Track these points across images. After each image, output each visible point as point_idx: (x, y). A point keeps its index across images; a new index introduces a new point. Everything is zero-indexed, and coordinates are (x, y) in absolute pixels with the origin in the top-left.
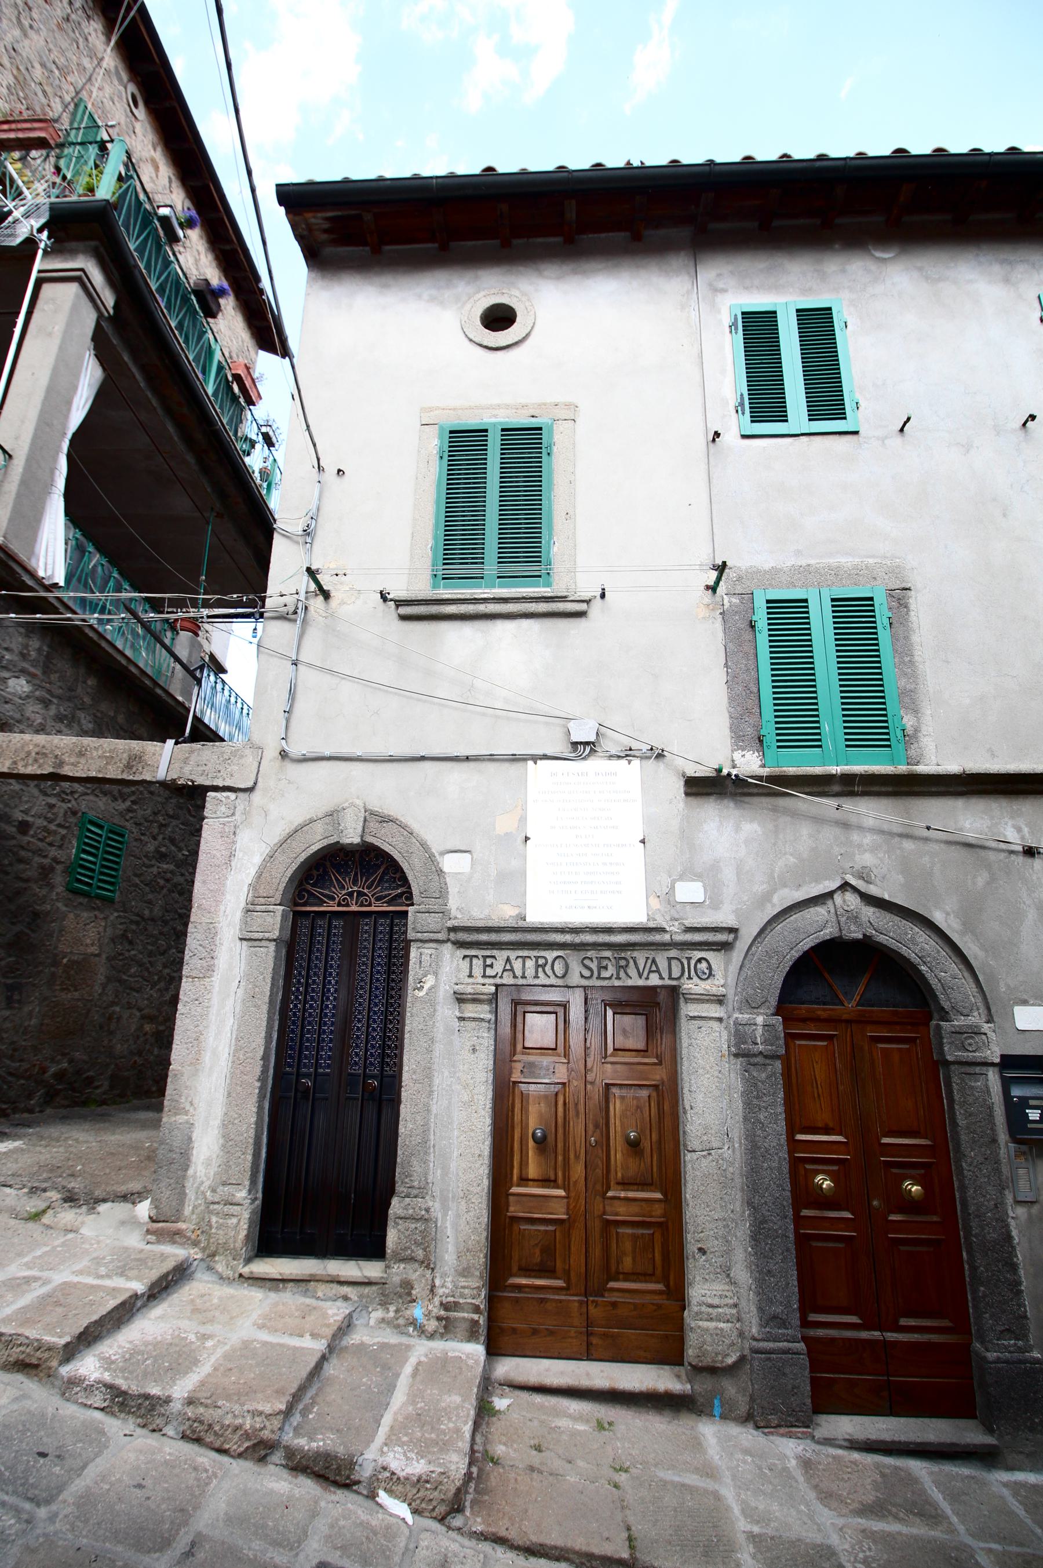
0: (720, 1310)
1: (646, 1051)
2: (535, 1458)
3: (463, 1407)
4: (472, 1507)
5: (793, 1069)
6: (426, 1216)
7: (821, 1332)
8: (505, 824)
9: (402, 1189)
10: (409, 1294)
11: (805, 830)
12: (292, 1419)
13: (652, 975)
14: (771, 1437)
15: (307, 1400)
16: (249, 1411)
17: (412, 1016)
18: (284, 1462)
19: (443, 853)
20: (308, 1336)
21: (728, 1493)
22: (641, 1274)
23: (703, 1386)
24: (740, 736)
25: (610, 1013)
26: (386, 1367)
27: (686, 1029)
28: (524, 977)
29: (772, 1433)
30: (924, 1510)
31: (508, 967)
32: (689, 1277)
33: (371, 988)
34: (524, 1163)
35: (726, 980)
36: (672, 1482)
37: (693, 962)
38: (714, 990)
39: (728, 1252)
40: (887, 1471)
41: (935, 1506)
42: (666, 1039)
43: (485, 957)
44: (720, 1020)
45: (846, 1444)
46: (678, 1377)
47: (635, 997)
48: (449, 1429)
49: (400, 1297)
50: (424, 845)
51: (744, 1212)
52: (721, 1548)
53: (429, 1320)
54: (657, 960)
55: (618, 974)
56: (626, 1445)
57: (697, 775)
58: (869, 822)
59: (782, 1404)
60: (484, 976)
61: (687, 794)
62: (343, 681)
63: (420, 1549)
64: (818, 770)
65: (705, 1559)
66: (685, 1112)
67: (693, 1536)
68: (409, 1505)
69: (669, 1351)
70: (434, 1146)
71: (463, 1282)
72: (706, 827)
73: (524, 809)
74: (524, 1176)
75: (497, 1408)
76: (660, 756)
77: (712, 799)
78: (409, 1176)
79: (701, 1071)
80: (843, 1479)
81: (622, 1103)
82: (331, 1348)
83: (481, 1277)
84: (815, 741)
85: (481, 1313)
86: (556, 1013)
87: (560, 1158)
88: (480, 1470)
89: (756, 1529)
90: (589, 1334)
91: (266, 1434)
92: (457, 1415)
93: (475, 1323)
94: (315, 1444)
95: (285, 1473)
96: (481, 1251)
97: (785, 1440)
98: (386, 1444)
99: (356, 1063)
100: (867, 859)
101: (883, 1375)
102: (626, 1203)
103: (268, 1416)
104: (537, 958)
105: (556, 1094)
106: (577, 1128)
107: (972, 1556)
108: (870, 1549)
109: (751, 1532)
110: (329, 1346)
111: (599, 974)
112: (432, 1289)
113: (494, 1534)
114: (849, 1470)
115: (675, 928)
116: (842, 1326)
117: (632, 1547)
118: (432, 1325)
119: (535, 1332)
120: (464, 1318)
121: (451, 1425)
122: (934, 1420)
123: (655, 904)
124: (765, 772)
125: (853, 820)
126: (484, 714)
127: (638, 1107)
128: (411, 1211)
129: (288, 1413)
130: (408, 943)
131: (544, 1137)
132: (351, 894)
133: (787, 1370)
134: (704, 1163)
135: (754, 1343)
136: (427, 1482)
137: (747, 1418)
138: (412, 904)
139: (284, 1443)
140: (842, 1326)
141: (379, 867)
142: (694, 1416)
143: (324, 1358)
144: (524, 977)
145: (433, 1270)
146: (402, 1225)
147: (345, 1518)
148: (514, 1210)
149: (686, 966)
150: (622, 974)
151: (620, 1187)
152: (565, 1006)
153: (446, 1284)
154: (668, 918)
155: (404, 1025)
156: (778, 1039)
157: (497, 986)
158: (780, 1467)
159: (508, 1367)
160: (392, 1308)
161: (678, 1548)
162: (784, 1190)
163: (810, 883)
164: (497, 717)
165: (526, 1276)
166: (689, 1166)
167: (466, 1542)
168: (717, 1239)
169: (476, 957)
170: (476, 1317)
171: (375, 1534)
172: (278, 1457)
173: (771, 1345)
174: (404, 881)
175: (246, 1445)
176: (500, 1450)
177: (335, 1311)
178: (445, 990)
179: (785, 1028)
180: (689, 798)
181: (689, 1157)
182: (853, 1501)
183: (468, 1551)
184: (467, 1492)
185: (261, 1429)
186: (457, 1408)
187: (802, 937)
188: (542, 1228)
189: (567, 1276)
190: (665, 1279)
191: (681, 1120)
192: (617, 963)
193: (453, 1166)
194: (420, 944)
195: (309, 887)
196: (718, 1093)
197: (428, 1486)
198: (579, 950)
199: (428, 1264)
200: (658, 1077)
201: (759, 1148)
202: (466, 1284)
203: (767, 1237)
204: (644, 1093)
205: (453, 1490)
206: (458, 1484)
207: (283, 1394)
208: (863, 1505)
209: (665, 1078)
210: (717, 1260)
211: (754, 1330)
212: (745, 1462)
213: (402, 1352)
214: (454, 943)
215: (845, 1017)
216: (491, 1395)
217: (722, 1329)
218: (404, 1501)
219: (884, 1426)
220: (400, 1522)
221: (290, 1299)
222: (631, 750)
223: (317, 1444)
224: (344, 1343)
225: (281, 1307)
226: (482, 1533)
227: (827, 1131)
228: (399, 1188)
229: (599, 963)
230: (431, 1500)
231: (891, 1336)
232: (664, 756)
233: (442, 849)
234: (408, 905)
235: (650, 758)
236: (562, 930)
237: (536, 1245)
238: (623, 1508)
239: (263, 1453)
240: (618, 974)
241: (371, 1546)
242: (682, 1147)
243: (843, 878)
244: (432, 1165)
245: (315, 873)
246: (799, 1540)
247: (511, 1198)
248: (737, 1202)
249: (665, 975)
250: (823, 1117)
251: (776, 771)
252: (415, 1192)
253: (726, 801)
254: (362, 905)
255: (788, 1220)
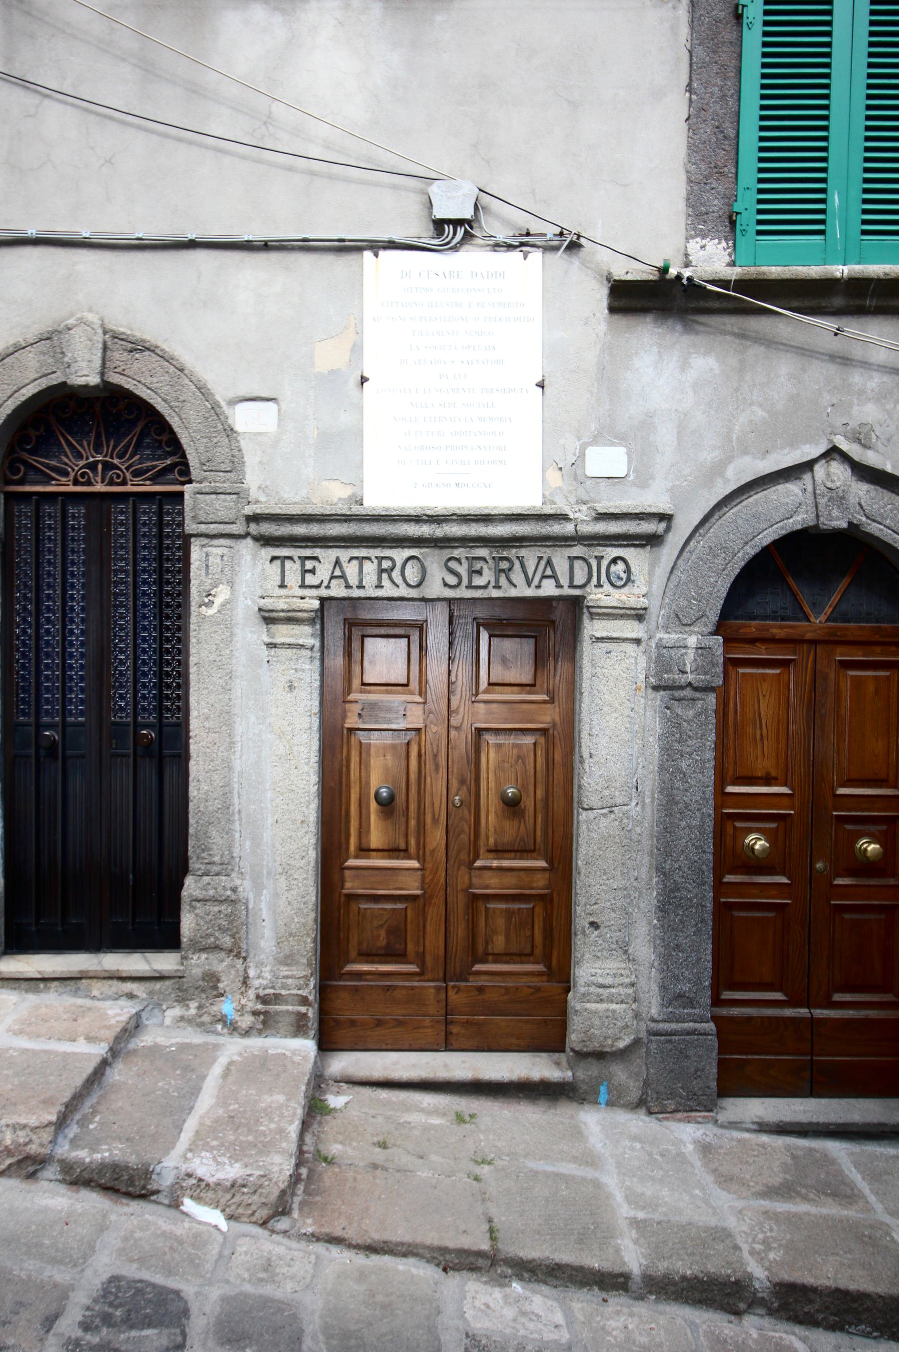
0: (613, 990)
1: (534, 685)
2: (379, 1155)
3: (287, 1106)
4: (301, 1209)
5: (731, 705)
6: (233, 897)
7: (735, 1011)
8: (329, 356)
9: (197, 866)
10: (215, 987)
11: (785, 367)
12: (67, 1131)
13: (546, 582)
14: (666, 1123)
15: (86, 1107)
16: (8, 1126)
17: (199, 642)
18: (60, 1177)
19: (232, 402)
20: (81, 1040)
21: (611, 1181)
22: (515, 954)
23: (585, 1073)
24: (701, 214)
25: (484, 636)
26: (188, 1068)
27: (588, 651)
28: (361, 587)
29: (667, 1119)
30: (839, 1190)
31: (338, 573)
32: (576, 954)
33: (135, 605)
34: (363, 830)
35: (650, 587)
36: (545, 1173)
37: (605, 563)
38: (633, 602)
39: (628, 925)
40: (800, 1153)
41: (852, 1186)
42: (562, 668)
43: (303, 559)
44: (638, 641)
45: (755, 1127)
46: (558, 1064)
47: (520, 613)
48: (270, 1130)
49: (203, 991)
50: (202, 389)
51: (651, 879)
52: (599, 1235)
53: (242, 1015)
54: (555, 561)
55: (497, 580)
56: (491, 1137)
57: (629, 277)
58: (880, 356)
59: (682, 1088)
60: (303, 586)
61: (612, 310)
62: (47, 102)
63: (236, 1254)
64: (814, 271)
65: (580, 1246)
66: (582, 762)
67: (566, 1225)
68: (223, 1211)
69: (550, 1037)
70: (239, 812)
71: (284, 971)
72: (637, 363)
73: (359, 333)
74: (364, 846)
75: (332, 1106)
76: (574, 246)
77: (649, 318)
78: (207, 849)
79: (606, 709)
80: (747, 1162)
81: (497, 752)
82: (115, 1052)
83: (309, 964)
84: (814, 224)
85: (310, 1005)
86: (408, 637)
87: (413, 823)
88: (311, 1172)
89: (641, 1215)
90: (447, 1023)
91: (33, 1149)
92: (281, 1116)
93: (304, 1016)
94: (99, 1156)
95: (62, 1189)
96: (308, 934)
97: (682, 1126)
98: (190, 1150)
99: (122, 709)
100: (868, 412)
101: (805, 1054)
102: (495, 874)
103: (34, 1129)
104: (380, 559)
105: (408, 744)
106: (436, 785)
107: (888, 1234)
108: (771, 1230)
109: (635, 1218)
110: (111, 1049)
111: (470, 581)
112: (245, 981)
113: (327, 1235)
114: (756, 1153)
115: (581, 514)
116: (764, 1004)
117: (493, 1239)
118: (246, 1021)
119: (379, 1023)
120: (287, 1012)
121: (273, 1126)
122: (861, 1100)
123: (555, 479)
124: (733, 273)
125: (857, 352)
126: (290, 169)
127: (519, 757)
128: (211, 892)
129: (61, 1123)
130: (186, 540)
131: (392, 798)
132: (93, 466)
133: (691, 1052)
134: (604, 823)
135: (653, 1025)
136: (244, 1186)
137: (641, 1104)
138: (190, 482)
139: (58, 1157)
140: (764, 1004)
141: (133, 424)
142: (575, 1104)
143: (104, 1064)
144: (361, 587)
145: (245, 959)
146: (200, 909)
147: (141, 1229)
148: (351, 886)
149: (595, 569)
150: (503, 581)
151: (491, 855)
152: (421, 627)
153: (263, 975)
154: (573, 500)
155: (188, 655)
156: (714, 665)
157: (323, 600)
158: (674, 1152)
159: (343, 1063)
160: (193, 1005)
161: (548, 1237)
162: (704, 852)
163: (782, 448)
164: (313, 174)
165: (367, 962)
166: (584, 827)
167: (294, 1244)
168: (614, 911)
169: (290, 558)
170: (303, 1009)
171: (181, 1243)
172: (51, 1172)
173: (673, 1026)
174: (174, 445)
175: (9, 1161)
176: (334, 1149)
177: (119, 1011)
178: (246, 607)
179: (726, 651)
180: (616, 317)
181: (584, 815)
182: (757, 1183)
183: (296, 1253)
184: (293, 1194)
185: (26, 1144)
186: (281, 1107)
187: (763, 526)
188: (389, 906)
189: (421, 959)
190: (547, 959)
191: (576, 772)
192: (497, 565)
193: (267, 836)
194: (205, 541)
195: (26, 456)
196: (627, 736)
197: (245, 1190)
198: (441, 548)
199: (237, 952)
200: (548, 719)
201: (677, 803)
202: (290, 973)
203: (677, 907)
204: (529, 740)
205: (276, 1193)
206: (282, 1186)
207: (53, 1104)
208: (768, 1187)
209: (557, 719)
210: (612, 935)
211: (654, 1011)
212: (632, 1149)
213: (209, 1053)
214: (256, 539)
215: (809, 636)
216: (324, 1092)
217: (614, 1011)
218: (217, 1207)
219: (802, 1108)
220: (212, 1229)
221: (54, 1000)
222: (528, 234)
223: (103, 1155)
224: (132, 1045)
225: (43, 1010)
226: (313, 1235)
227: (768, 781)
228: (194, 864)
229: (470, 566)
230: (250, 1205)
231: (819, 1013)
232: (580, 246)
233: (231, 395)
234: (183, 483)
235: (556, 249)
236: (417, 519)
237: (381, 926)
238: (484, 1200)
239: (31, 1169)
240: (497, 580)
241: (176, 1256)
242: (575, 805)
243: (830, 441)
244: (237, 835)
245: (33, 433)
246: (690, 1224)
247: (347, 873)
248: (643, 866)
249: (564, 581)
250: (764, 764)
251: (752, 271)
252: (216, 869)
253: (670, 322)
254: (111, 483)
255: (706, 887)
